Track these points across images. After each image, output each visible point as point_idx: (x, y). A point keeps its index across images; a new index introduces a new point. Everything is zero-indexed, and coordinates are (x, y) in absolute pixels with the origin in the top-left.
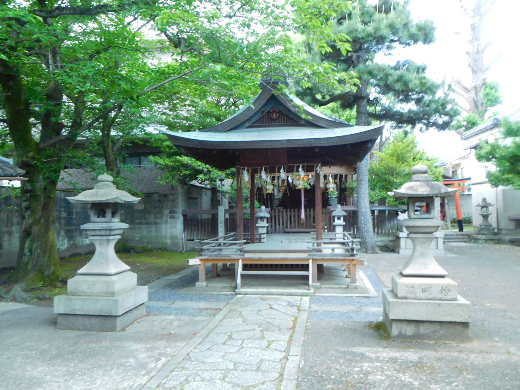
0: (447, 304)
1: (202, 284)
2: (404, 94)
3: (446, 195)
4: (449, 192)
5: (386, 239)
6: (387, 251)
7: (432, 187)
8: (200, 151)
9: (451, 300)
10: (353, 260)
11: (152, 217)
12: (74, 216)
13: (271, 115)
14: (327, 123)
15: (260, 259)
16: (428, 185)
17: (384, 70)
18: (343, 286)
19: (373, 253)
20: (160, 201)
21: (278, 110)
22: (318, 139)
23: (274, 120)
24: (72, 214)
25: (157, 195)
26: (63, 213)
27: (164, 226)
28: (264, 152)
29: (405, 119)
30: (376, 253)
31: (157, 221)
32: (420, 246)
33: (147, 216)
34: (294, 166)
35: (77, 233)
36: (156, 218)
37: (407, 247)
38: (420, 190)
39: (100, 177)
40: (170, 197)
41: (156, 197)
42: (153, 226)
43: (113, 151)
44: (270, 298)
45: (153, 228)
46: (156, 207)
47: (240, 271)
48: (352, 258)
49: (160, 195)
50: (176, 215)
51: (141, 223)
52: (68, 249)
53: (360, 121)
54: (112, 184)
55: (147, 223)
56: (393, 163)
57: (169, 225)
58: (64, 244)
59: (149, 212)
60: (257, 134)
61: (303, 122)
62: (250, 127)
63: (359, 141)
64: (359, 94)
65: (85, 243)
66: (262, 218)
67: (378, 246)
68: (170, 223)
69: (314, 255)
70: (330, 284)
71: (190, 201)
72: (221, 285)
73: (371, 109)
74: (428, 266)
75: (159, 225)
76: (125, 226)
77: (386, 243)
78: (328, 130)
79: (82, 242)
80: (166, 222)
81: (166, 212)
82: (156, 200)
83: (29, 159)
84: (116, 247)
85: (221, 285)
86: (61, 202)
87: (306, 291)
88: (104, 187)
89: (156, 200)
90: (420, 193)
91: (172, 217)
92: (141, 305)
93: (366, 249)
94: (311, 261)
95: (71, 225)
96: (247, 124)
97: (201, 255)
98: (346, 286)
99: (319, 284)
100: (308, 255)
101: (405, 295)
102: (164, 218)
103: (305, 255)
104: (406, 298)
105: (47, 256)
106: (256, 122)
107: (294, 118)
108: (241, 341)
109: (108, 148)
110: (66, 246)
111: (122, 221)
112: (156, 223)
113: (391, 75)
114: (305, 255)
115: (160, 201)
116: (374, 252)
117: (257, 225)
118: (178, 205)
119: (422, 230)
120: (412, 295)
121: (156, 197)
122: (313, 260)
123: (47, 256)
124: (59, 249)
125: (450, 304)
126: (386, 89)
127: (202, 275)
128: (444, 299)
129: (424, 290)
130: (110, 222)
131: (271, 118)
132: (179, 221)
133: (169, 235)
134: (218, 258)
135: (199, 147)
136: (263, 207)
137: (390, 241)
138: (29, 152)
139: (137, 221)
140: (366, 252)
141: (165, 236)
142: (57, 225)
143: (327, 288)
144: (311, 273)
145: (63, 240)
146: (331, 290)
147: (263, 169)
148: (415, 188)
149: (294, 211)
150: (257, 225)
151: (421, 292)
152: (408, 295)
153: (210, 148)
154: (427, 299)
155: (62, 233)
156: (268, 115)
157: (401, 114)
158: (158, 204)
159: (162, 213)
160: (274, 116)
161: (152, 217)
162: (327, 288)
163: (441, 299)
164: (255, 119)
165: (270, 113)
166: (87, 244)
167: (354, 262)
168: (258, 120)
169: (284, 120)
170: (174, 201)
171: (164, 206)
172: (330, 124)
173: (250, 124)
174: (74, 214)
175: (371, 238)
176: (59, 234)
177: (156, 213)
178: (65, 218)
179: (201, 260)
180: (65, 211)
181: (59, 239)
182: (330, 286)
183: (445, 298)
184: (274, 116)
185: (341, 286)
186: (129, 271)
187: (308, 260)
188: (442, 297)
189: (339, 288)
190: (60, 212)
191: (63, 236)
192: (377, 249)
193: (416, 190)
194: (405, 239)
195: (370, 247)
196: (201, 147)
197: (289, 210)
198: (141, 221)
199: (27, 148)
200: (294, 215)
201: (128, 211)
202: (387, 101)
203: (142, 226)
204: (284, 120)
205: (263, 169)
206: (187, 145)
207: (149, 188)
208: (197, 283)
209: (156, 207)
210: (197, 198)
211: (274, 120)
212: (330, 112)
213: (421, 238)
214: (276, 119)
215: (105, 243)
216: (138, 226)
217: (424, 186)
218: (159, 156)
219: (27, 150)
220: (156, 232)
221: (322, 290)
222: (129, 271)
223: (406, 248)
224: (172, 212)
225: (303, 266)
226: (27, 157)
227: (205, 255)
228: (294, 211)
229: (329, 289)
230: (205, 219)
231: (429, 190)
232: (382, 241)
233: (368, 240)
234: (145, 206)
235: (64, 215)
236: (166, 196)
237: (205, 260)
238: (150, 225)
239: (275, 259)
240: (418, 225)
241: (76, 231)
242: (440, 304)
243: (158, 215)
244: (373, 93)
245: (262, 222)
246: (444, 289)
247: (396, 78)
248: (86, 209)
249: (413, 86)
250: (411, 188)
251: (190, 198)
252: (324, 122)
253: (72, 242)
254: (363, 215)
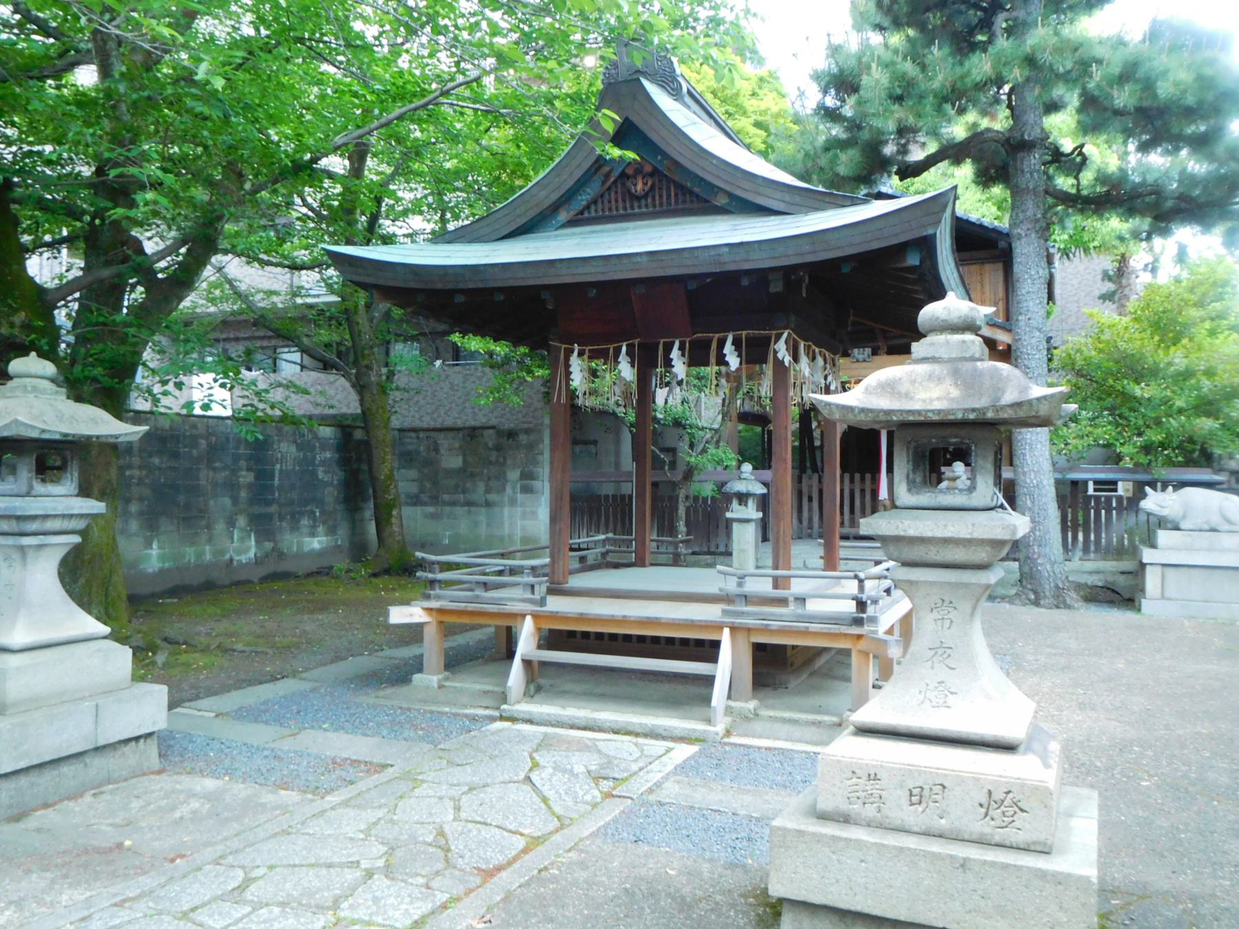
0: (993, 864)
1: (428, 680)
2: (1155, 121)
3: (1022, 414)
4: (1030, 402)
5: (1110, 565)
6: (1111, 603)
7: (969, 383)
8: (459, 299)
9: (1026, 849)
10: (859, 637)
11: (481, 487)
12: (276, 482)
13: (629, 184)
14: (787, 198)
15: (582, 618)
16: (956, 374)
17: (1076, 49)
18: (826, 718)
19: (1058, 607)
20: (498, 448)
21: (648, 169)
22: (741, 244)
23: (638, 198)
24: (272, 477)
25: (491, 431)
26: (244, 473)
27: (506, 511)
28: (593, 293)
29: (1169, 204)
30: (1069, 607)
31: (492, 497)
32: (935, 615)
33: (469, 485)
34: (710, 341)
35: (284, 524)
36: (488, 490)
37: (1167, 594)
38: (922, 395)
39: (16, 365)
40: (523, 438)
41: (489, 438)
42: (483, 510)
43: (371, 321)
44: (579, 741)
45: (482, 515)
46: (491, 463)
47: (526, 643)
48: (855, 630)
49: (500, 433)
50: (537, 484)
51: (453, 504)
52: (258, 561)
53: (1021, 216)
54: (53, 387)
55: (469, 504)
56: (1141, 343)
57: (519, 509)
58: (248, 550)
59: (472, 475)
60: (576, 240)
61: (722, 201)
62: (572, 223)
63: (875, 245)
64: (1017, 135)
65: (306, 549)
66: (742, 498)
67: (1079, 587)
68: (523, 505)
69: (742, 614)
70: (790, 709)
71: (578, 449)
72: (478, 687)
73: (1064, 183)
74: (951, 700)
75: (496, 510)
76: (96, 506)
77: (1110, 579)
78: (788, 219)
79: (300, 545)
80: (513, 502)
81: (513, 475)
82: (490, 445)
83: (16, 331)
84: (64, 563)
85: (478, 687)
86: (237, 448)
87: (700, 726)
88: (18, 393)
89: (490, 445)
90: (917, 406)
91: (527, 490)
92: (127, 741)
93: (1035, 592)
94: (726, 631)
95: (268, 503)
96: (563, 216)
97: (428, 597)
98: (835, 719)
99: (752, 705)
100: (724, 611)
101: (844, 807)
102: (509, 490)
103: (712, 612)
104: (845, 819)
105: (82, 580)
106: (588, 207)
107: (696, 190)
108: (249, 909)
109: (356, 313)
110: (251, 554)
111: (84, 491)
112: (488, 504)
113: (1099, 62)
114: (712, 612)
115: (498, 448)
116: (1060, 603)
117: (729, 515)
118: (540, 458)
119: (934, 554)
120: (870, 811)
121: (489, 438)
122: (734, 629)
123: (82, 580)
124: (231, 560)
125: (1005, 866)
126: (1097, 112)
127: (432, 648)
128: (997, 839)
129: (917, 797)
130: (28, 494)
131: (629, 191)
132: (543, 499)
133: (518, 534)
134: (471, 607)
135: (412, 285)
136: (747, 467)
137: (1123, 573)
138: (17, 310)
139: (446, 497)
140: (1036, 603)
141: (510, 536)
142: (227, 501)
143: (776, 719)
144: (728, 664)
145: (242, 539)
146: (786, 728)
147: (624, 349)
148: (904, 388)
149: (863, 479)
150: (729, 515)
151: (904, 801)
152: (856, 807)
153: (439, 286)
154: (927, 834)
155: (242, 521)
156: (623, 184)
157: (1157, 191)
158: (494, 456)
159: (501, 477)
160: (640, 186)
161: (481, 487)
162: (776, 719)
163: (982, 842)
164: (583, 199)
165: (628, 177)
166: (313, 550)
167: (862, 645)
168: (595, 202)
169: (669, 196)
170: (531, 447)
171: (509, 462)
172: (798, 199)
173: (572, 213)
174: (277, 475)
175: (1053, 564)
176: (231, 523)
177: (489, 479)
178: (250, 486)
179: (429, 610)
180: (249, 469)
181: (232, 538)
182: (787, 715)
183: (999, 835)
184: (640, 186)
185: (819, 718)
186: (105, 637)
187: (719, 627)
188: (987, 830)
189: (813, 723)
190: (234, 472)
191: (242, 530)
192: (1072, 597)
193: (907, 396)
194: (1159, 569)
195: (1048, 589)
196: (421, 286)
197: (857, 476)
198: (456, 497)
199: (10, 301)
200: (863, 491)
201: (426, 471)
202: (1108, 156)
203: (459, 510)
204: (669, 196)
205: (624, 349)
206: (381, 282)
207: (503, 416)
208: (417, 677)
209: (491, 463)
210: (595, 443)
211: (638, 198)
212: (994, 209)
213: (932, 583)
214: (645, 196)
215: (16, 556)
216: (448, 509)
217: (940, 380)
218: (251, 307)
219: (10, 306)
220: (488, 525)
221: (758, 726)
222: (105, 637)
223: (1163, 597)
224: (527, 476)
225: (700, 643)
226: (12, 325)
227: (438, 598)
228: (863, 479)
229: (777, 726)
230: (607, 497)
231: (955, 393)
232: (1097, 572)
233: (1044, 567)
234: (465, 461)
235: (247, 477)
236: (511, 434)
237: (441, 611)
238: (472, 509)
239: (624, 621)
240: (939, 533)
241: (281, 518)
242: (964, 864)
243: (493, 483)
244: (1062, 128)
245: (743, 507)
246: (1001, 801)
247: (1116, 70)
248: (313, 464)
249: (1171, 90)
250: (889, 388)
251: (575, 442)
252: (778, 195)
253: (268, 545)
254: (1031, 495)
